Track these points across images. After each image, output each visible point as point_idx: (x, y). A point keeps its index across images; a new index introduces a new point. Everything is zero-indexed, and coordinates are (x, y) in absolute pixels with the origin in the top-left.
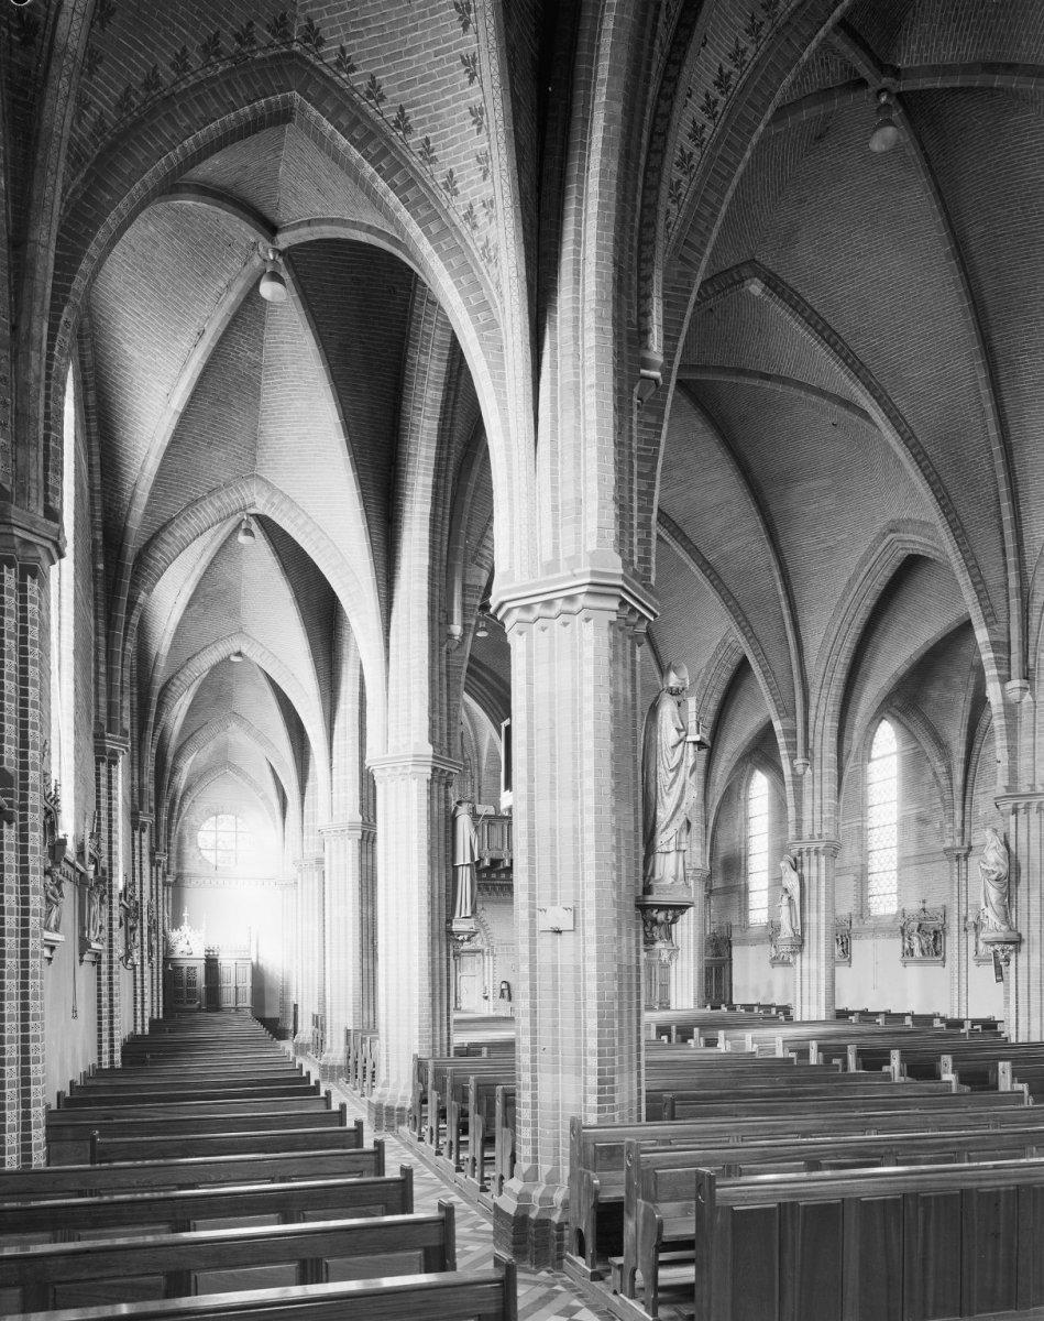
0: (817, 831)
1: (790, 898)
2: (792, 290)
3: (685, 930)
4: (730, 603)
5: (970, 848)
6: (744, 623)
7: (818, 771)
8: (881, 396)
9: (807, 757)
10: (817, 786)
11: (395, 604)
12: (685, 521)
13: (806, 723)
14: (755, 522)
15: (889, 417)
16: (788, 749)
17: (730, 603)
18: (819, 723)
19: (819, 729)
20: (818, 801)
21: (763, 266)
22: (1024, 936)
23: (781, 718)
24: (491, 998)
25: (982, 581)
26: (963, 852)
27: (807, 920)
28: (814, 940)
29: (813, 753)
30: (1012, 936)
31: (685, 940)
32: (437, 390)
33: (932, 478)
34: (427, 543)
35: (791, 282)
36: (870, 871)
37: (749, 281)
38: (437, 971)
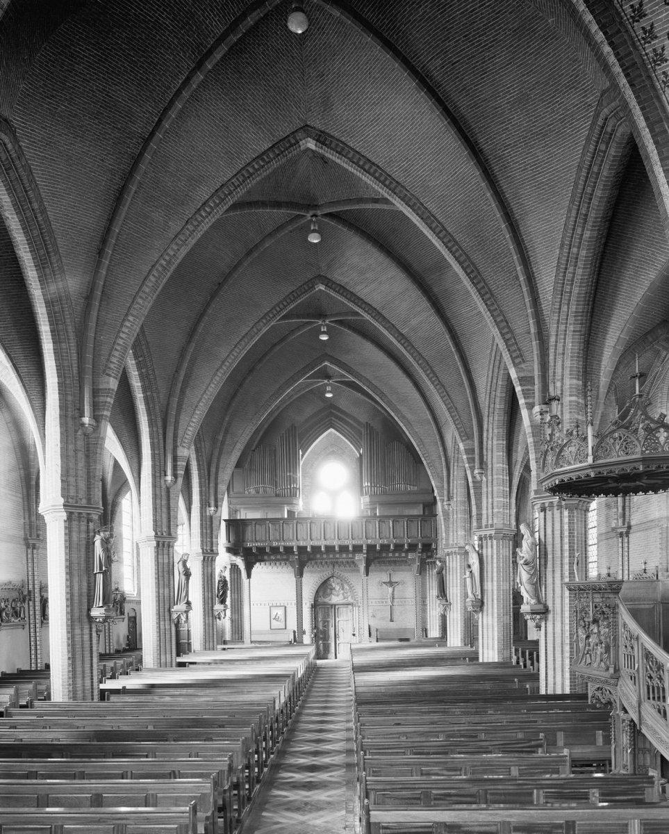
0: (490, 522)
1: (471, 572)
2: (338, 140)
3: (455, 591)
4: (420, 362)
5: (629, 527)
6: (431, 375)
7: (490, 478)
8: (415, 204)
9: (481, 468)
10: (490, 489)
11: (47, 409)
12: (383, 308)
13: (481, 443)
14: (424, 303)
15: (422, 219)
16: (469, 463)
17: (420, 362)
18: (490, 442)
19: (490, 447)
20: (490, 500)
21: (314, 128)
22: (551, 608)
23: (463, 441)
24: (357, 635)
25: (511, 331)
26: (624, 530)
27: (485, 587)
28: (490, 603)
29: (486, 464)
30: (541, 607)
31: (455, 599)
32: (32, 270)
33: (462, 259)
34: (55, 368)
35: (336, 134)
36: (337, 567)
37: (304, 141)
38: (78, 646)
